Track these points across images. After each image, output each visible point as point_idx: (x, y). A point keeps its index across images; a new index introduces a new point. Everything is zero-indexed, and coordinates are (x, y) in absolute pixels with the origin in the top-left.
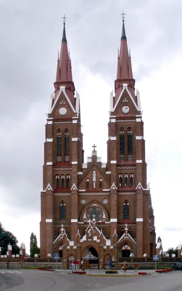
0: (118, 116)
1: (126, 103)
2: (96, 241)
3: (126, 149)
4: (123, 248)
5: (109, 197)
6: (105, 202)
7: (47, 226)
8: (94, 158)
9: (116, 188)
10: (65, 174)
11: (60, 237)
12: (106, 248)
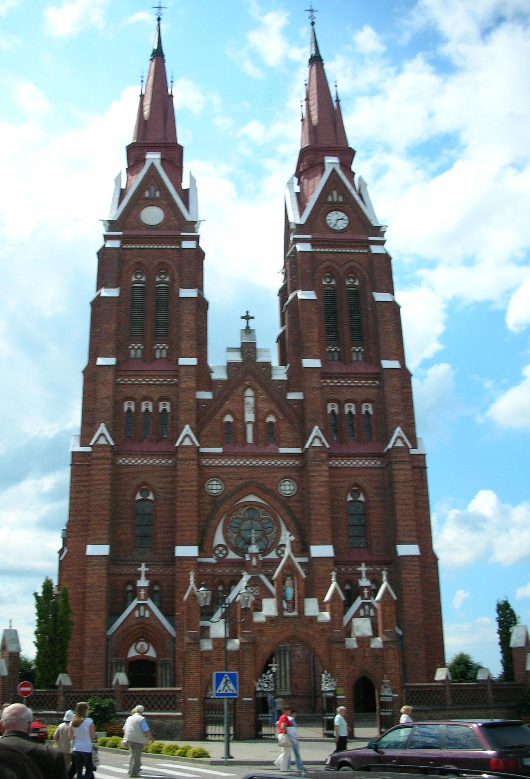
0: (318, 236)
1: (338, 203)
2: (315, 617)
3: (346, 328)
4: (132, 653)
5: (301, 469)
6: (287, 488)
7: (89, 570)
8: (248, 349)
9: (323, 443)
10: (156, 397)
11: (133, 611)
12: (355, 646)
